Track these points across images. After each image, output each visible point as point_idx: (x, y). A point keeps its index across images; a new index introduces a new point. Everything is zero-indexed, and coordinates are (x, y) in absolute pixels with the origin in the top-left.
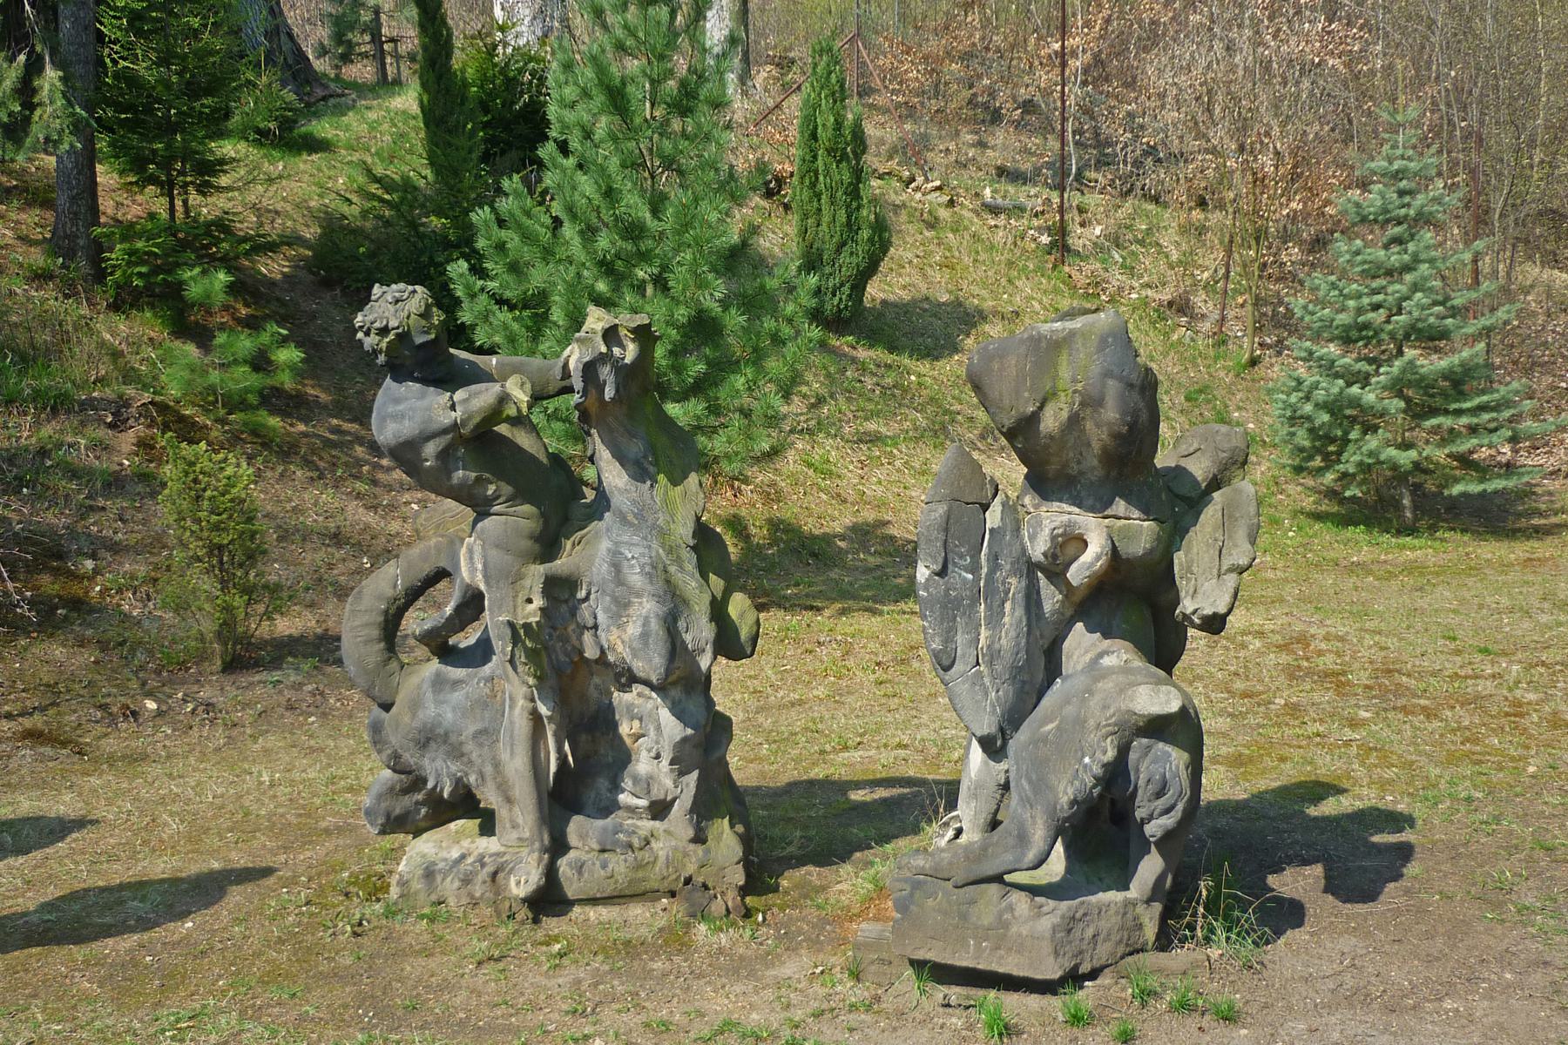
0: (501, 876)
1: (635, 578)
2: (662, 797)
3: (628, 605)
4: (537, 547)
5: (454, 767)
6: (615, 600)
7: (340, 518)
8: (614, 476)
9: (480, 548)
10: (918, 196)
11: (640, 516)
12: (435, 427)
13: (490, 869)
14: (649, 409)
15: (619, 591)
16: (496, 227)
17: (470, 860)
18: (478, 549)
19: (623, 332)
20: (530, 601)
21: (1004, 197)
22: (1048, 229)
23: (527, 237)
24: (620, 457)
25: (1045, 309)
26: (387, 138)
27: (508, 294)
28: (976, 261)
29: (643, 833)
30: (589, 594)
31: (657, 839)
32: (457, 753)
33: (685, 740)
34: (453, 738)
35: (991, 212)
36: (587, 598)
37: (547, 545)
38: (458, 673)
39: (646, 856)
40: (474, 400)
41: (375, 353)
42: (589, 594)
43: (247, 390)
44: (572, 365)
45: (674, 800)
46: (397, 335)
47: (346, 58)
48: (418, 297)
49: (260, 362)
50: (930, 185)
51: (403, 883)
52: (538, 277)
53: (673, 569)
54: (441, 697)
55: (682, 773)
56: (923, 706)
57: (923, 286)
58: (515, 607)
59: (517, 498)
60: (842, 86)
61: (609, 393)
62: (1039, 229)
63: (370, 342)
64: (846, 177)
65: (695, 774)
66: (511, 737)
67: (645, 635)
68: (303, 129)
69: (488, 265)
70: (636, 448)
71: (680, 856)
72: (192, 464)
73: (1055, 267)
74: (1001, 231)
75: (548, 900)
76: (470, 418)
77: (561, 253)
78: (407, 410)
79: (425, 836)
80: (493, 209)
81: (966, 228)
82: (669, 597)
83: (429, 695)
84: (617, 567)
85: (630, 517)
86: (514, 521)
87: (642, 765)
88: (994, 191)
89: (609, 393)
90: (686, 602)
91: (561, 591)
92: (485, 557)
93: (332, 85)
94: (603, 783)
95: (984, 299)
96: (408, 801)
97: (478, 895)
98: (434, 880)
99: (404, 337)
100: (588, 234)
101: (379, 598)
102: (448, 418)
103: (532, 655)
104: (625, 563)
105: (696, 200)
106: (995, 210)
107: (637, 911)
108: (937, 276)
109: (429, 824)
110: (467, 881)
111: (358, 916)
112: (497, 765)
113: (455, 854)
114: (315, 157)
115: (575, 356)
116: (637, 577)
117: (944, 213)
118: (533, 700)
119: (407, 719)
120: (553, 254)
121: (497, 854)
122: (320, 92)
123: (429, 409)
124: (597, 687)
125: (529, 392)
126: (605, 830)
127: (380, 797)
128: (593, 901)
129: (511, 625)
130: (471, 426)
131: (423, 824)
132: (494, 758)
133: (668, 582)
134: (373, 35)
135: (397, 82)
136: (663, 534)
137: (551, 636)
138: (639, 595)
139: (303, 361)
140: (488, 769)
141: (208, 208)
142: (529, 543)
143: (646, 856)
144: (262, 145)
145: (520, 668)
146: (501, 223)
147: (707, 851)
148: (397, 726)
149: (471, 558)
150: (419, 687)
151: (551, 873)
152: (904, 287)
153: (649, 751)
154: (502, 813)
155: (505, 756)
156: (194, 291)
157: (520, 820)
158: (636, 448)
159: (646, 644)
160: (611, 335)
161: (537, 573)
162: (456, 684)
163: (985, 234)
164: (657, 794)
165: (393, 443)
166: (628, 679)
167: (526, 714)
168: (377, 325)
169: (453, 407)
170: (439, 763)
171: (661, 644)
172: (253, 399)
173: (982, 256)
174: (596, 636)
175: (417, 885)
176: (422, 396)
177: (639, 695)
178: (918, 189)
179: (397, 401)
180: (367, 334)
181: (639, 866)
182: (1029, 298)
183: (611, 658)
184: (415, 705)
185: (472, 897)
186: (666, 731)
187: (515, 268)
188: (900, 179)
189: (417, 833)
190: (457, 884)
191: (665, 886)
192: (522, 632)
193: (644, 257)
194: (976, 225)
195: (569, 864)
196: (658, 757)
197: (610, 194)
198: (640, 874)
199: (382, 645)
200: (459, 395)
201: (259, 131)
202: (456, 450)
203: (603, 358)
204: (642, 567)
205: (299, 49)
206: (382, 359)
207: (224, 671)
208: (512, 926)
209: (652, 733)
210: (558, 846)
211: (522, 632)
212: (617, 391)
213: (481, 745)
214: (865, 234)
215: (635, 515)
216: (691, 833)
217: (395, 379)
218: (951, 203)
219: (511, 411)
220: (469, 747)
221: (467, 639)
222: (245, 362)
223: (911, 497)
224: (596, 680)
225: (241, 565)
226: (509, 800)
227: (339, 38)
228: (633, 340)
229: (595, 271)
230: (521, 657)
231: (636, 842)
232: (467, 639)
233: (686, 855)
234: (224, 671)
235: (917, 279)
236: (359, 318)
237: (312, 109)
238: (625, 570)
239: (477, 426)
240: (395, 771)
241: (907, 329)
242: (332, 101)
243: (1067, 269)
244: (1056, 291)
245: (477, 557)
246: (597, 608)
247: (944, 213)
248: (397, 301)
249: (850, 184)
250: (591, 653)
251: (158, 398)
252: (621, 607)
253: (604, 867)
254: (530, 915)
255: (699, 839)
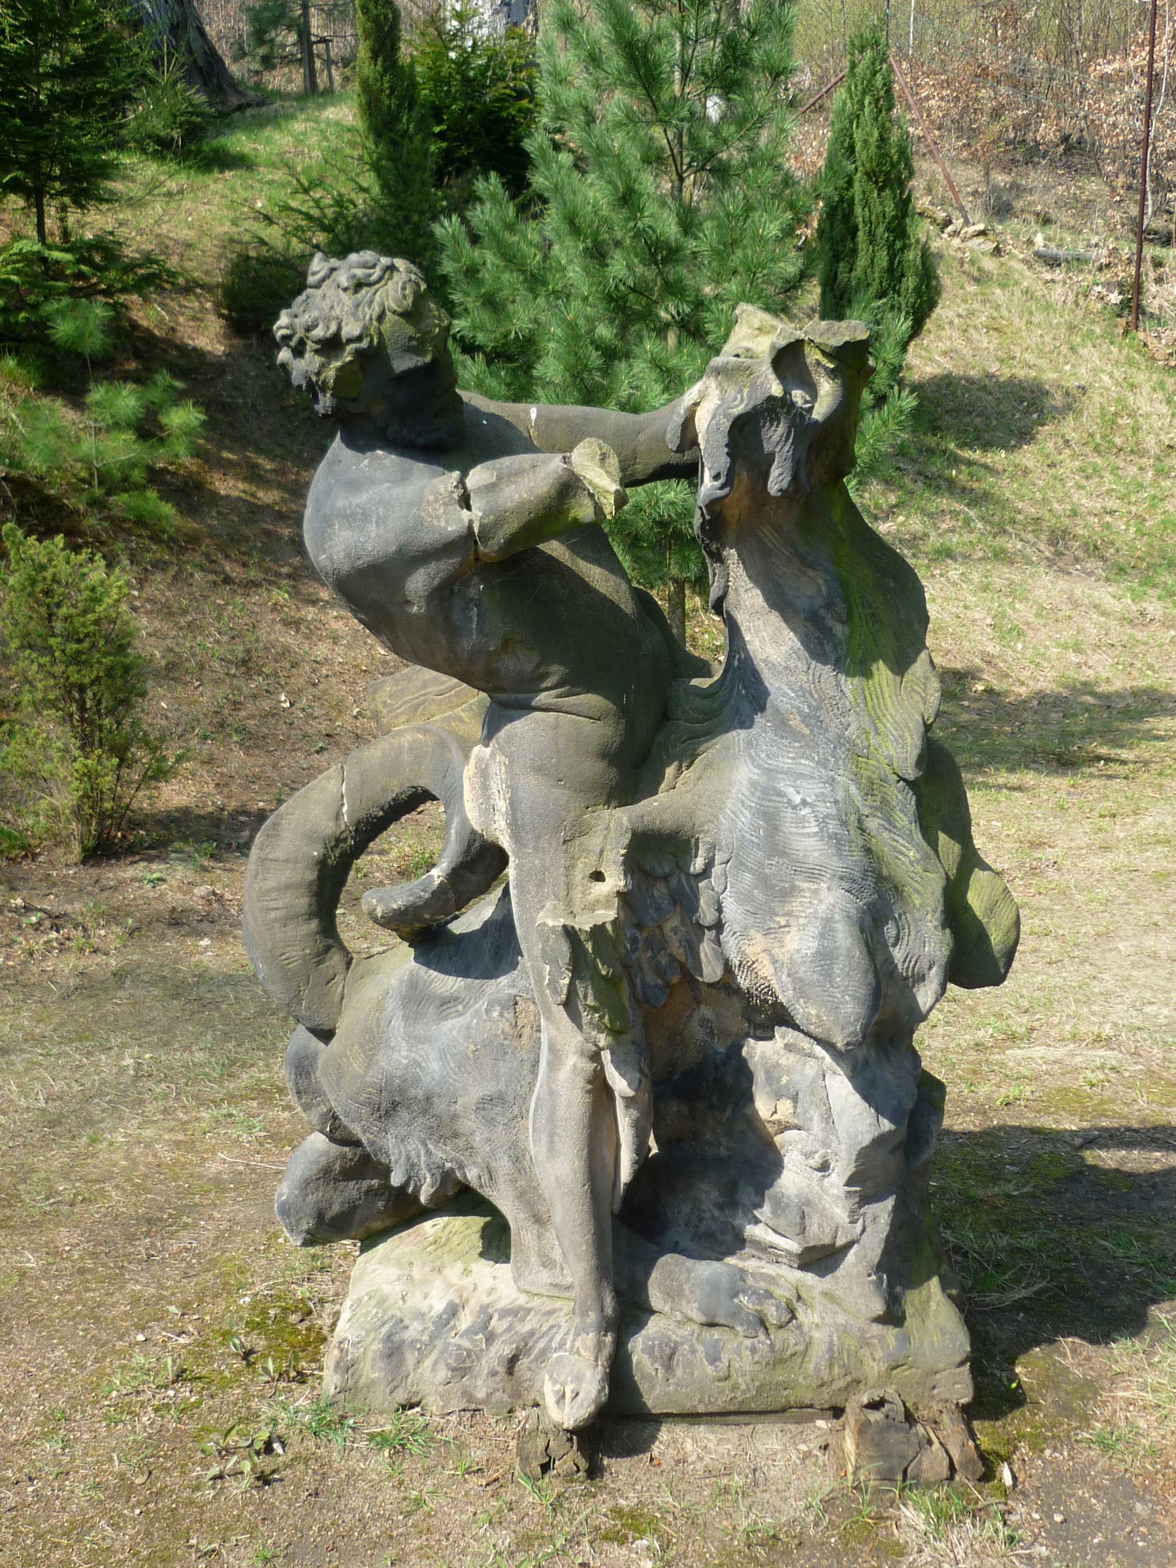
0: (523, 1363)
1: (808, 842)
2: (827, 1240)
3: (789, 893)
4: (613, 774)
5: (442, 1154)
6: (764, 881)
7: (250, 637)
8: (771, 642)
9: (500, 773)
10: (956, 242)
11: (813, 719)
12: (428, 538)
13: (503, 1349)
14: (836, 514)
15: (772, 866)
16: (467, 246)
17: (465, 1321)
18: (498, 773)
19: (813, 356)
20: (598, 876)
21: (1059, 246)
22: (1120, 285)
23: (510, 258)
24: (778, 600)
25: (1117, 384)
26: (317, 153)
27: (481, 338)
28: (1029, 323)
29: (782, 1293)
30: (709, 865)
31: (808, 1306)
32: (445, 1130)
33: (879, 1141)
34: (440, 1106)
35: (1046, 263)
36: (706, 873)
37: (631, 769)
38: (449, 984)
39: (788, 1339)
40: (503, 489)
41: (313, 389)
42: (709, 865)
43: (133, 465)
44: (702, 422)
45: (848, 1246)
46: (358, 353)
47: (268, 62)
48: (399, 279)
49: (148, 428)
50: (971, 229)
51: (346, 1367)
52: (523, 315)
53: (873, 824)
54: (420, 1029)
55: (866, 1199)
56: (1096, 956)
57: (967, 352)
58: (569, 887)
59: (575, 682)
60: (889, 91)
61: (778, 479)
62: (1107, 285)
63: (303, 367)
64: (890, 209)
65: (890, 1203)
66: (551, 1119)
67: (825, 957)
68: (215, 143)
69: (456, 297)
70: (811, 588)
71: (851, 1343)
72: (43, 568)
73: (1126, 332)
74: (1059, 288)
75: (618, 1425)
76: (498, 523)
77: (555, 282)
78: (374, 503)
79: (381, 1248)
80: (465, 221)
81: (1016, 283)
82: (870, 882)
83: (398, 1024)
84: (770, 820)
85: (795, 722)
86: (564, 726)
87: (794, 1178)
88: (1048, 239)
89: (778, 479)
90: (897, 890)
91: (662, 865)
92: (513, 788)
93: (252, 93)
94: (707, 1193)
95: (1041, 370)
96: (353, 1189)
97: (480, 1394)
98: (401, 1362)
99: (372, 357)
100: (598, 254)
101: (311, 837)
102: (452, 522)
103: (607, 989)
104: (789, 813)
105: (748, 209)
106: (1052, 262)
107: (770, 1443)
108: (985, 341)
109: (388, 1222)
110: (461, 1370)
111: (264, 1435)
112: (518, 1158)
113: (438, 1304)
114: (228, 174)
115: (710, 405)
116: (812, 842)
117: (989, 264)
118: (595, 1057)
119: (357, 1066)
120: (545, 283)
121: (515, 1313)
122: (234, 101)
123: (418, 502)
124: (704, 1022)
125: (617, 475)
126: (714, 1285)
127: (306, 1184)
128: (691, 1417)
129: (570, 934)
130: (501, 537)
131: (378, 1225)
132: (514, 1145)
133: (868, 851)
134: (300, 35)
135: (329, 92)
136: (857, 754)
137: (634, 941)
138: (813, 875)
139: (203, 424)
140: (503, 1165)
141: (93, 222)
142: (600, 766)
143: (788, 1339)
144: (163, 158)
145: (585, 1017)
146: (475, 239)
147: (906, 1340)
148: (340, 1077)
149: (485, 787)
150: (380, 1007)
151: (618, 1373)
152: (945, 353)
153: (808, 1155)
154: (522, 1232)
155: (536, 1149)
156: (63, 329)
157: (557, 1255)
158: (811, 588)
159: (828, 975)
160: (788, 359)
161: (613, 827)
162: (447, 1003)
163: (1039, 289)
164: (819, 1234)
165: (346, 567)
166: (771, 1017)
167: (580, 1083)
168: (319, 332)
169: (465, 501)
170: (413, 1146)
171: (857, 976)
172: (137, 475)
173: (1038, 318)
174: (718, 942)
175: (371, 1371)
176: (403, 478)
177: (789, 1047)
178: (956, 233)
179: (354, 486)
180: (299, 352)
181: (779, 1360)
182: (1096, 371)
183: (744, 981)
184: (373, 1042)
185: (471, 1399)
186: (843, 1124)
187: (493, 303)
188: (934, 221)
189: (369, 1241)
190: (443, 1373)
191: (825, 1398)
192: (589, 946)
193: (673, 289)
194: (1028, 278)
195: (649, 1350)
196: (824, 1167)
197: (628, 199)
198: (780, 1376)
199: (314, 924)
200: (478, 476)
201: (159, 141)
202: (466, 584)
203: (772, 409)
204: (822, 822)
205: (212, 49)
206: (325, 403)
207: (84, 862)
208: (552, 1485)
209: (817, 1125)
210: (627, 1312)
211: (589, 946)
212: (795, 478)
213: (491, 1123)
214: (910, 282)
215: (805, 718)
216: (878, 1307)
217: (352, 442)
218: (997, 252)
219: (583, 511)
220: (470, 1123)
221: (472, 919)
222: (129, 426)
223: (974, 621)
224: (706, 1011)
225: (110, 712)
226: (539, 1220)
227: (260, 36)
228: (832, 374)
229: (601, 307)
230: (588, 997)
231: (772, 1314)
232: (472, 919)
233: (865, 1343)
234: (84, 862)
235: (959, 343)
236: (284, 319)
237: (225, 119)
238: (788, 827)
239: (512, 540)
240: (332, 1139)
241: (951, 405)
242: (249, 112)
243: (1141, 335)
244: (1130, 362)
245: (497, 784)
246: (727, 894)
247: (989, 264)
248: (359, 285)
249: (894, 217)
250: (711, 972)
251: (15, 473)
252: (775, 895)
253: (714, 1359)
254: (583, 1464)
255: (893, 1316)
